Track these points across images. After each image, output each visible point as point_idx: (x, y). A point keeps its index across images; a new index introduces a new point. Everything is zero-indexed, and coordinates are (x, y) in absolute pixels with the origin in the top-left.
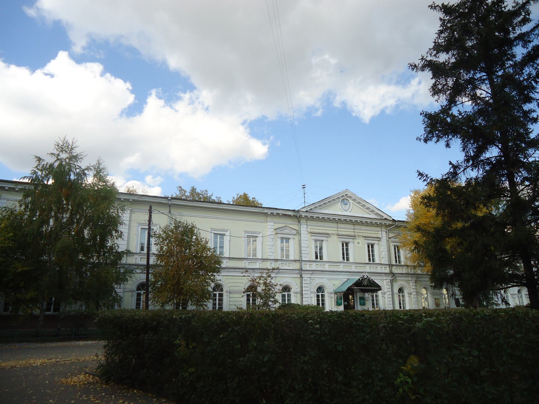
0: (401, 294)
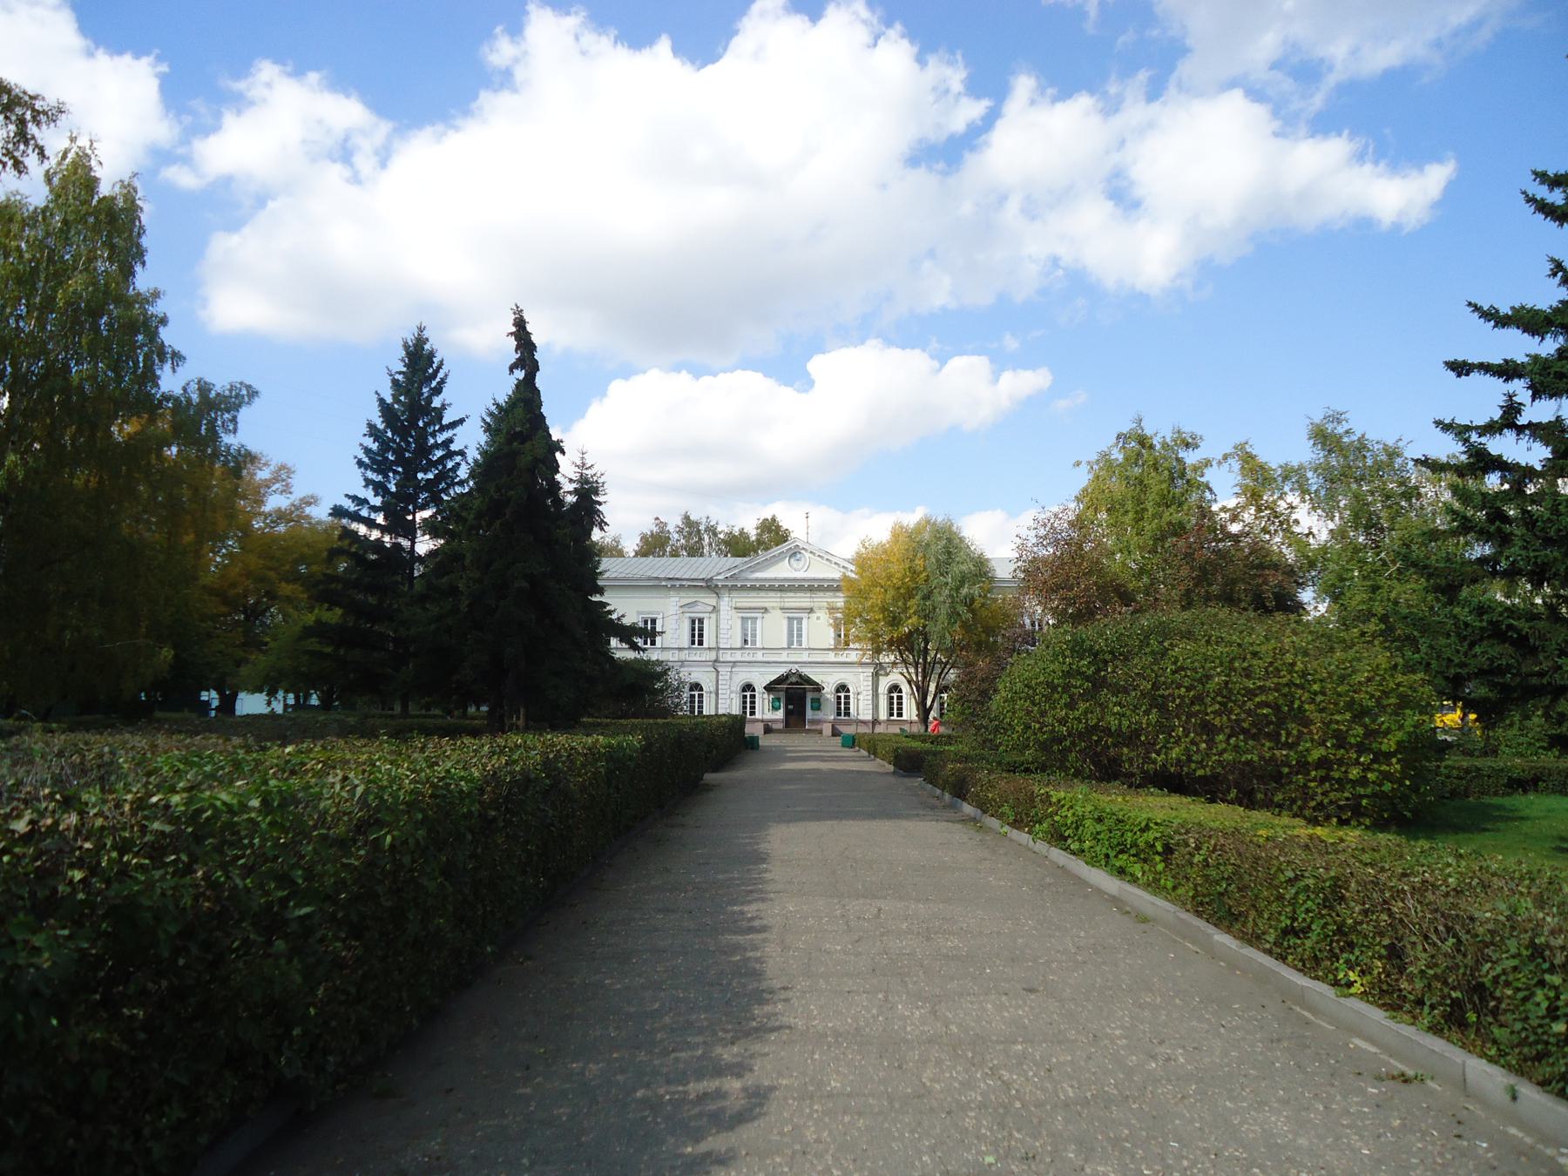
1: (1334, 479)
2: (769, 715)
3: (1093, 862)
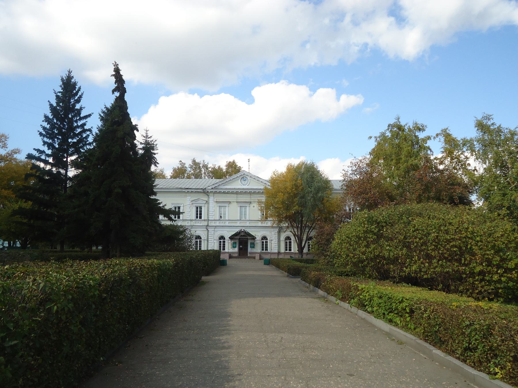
1: (487, 145)
2: (231, 250)
3: (378, 316)
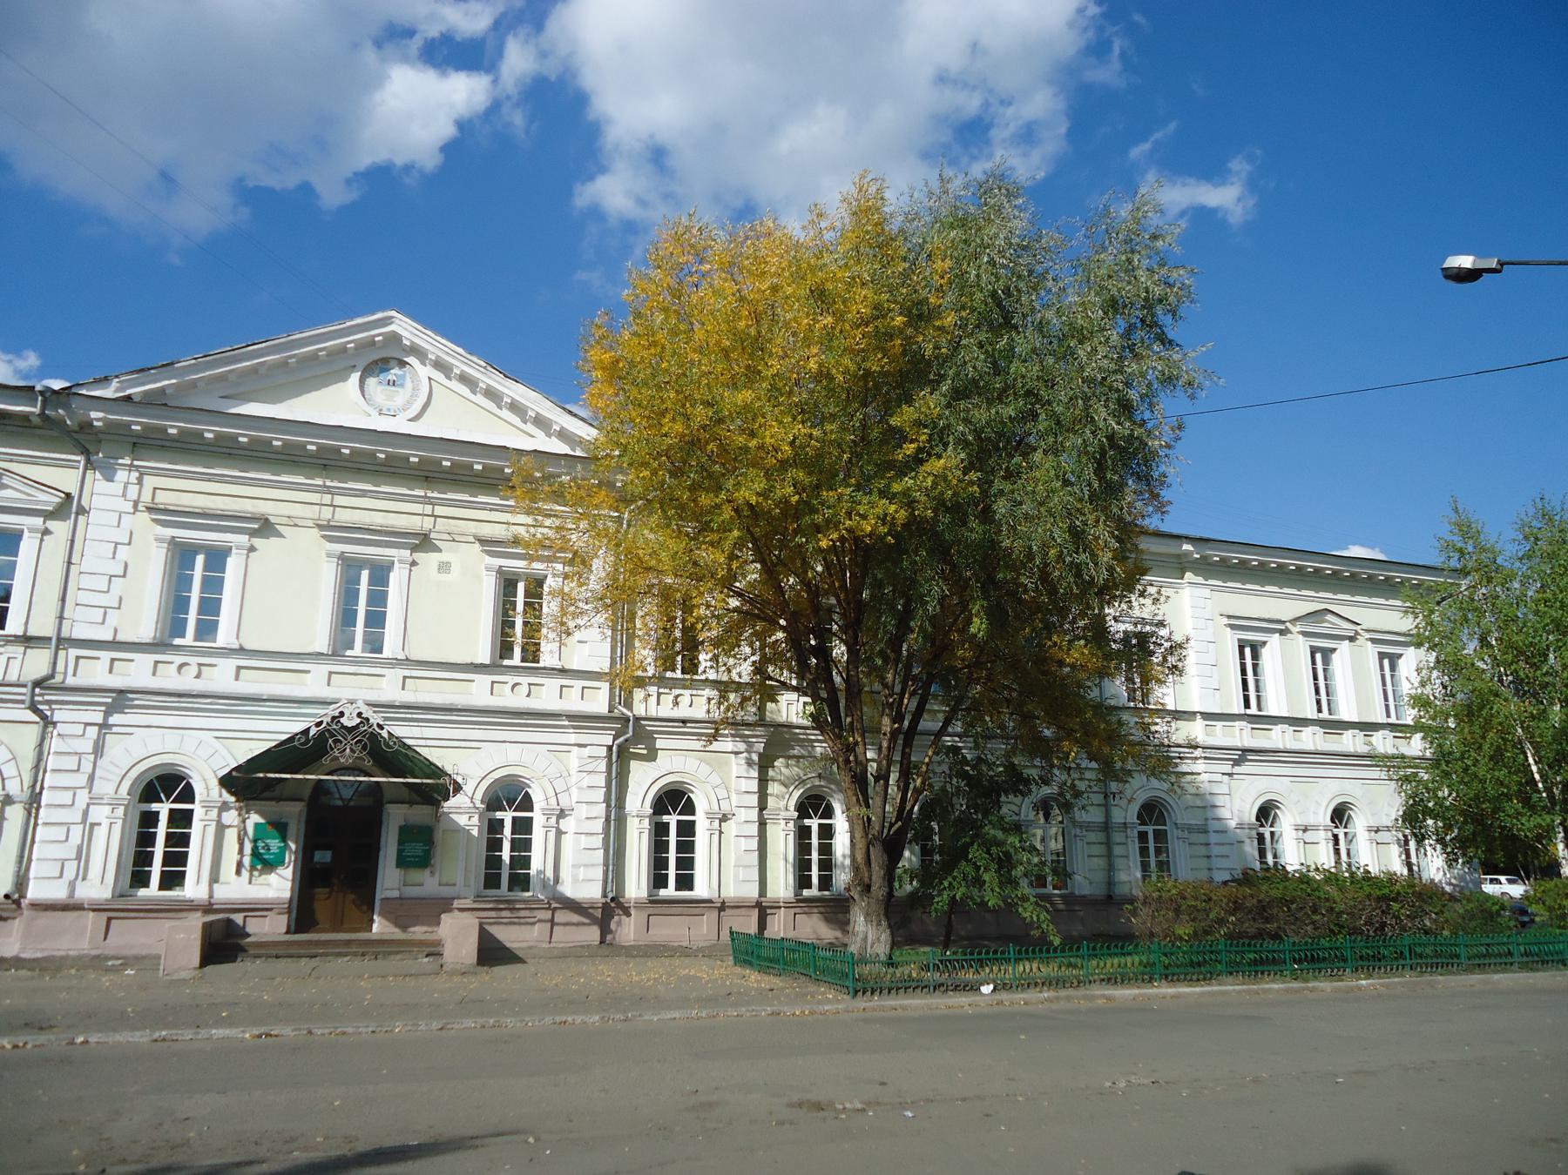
0: (1340, 832)
2: (236, 888)
